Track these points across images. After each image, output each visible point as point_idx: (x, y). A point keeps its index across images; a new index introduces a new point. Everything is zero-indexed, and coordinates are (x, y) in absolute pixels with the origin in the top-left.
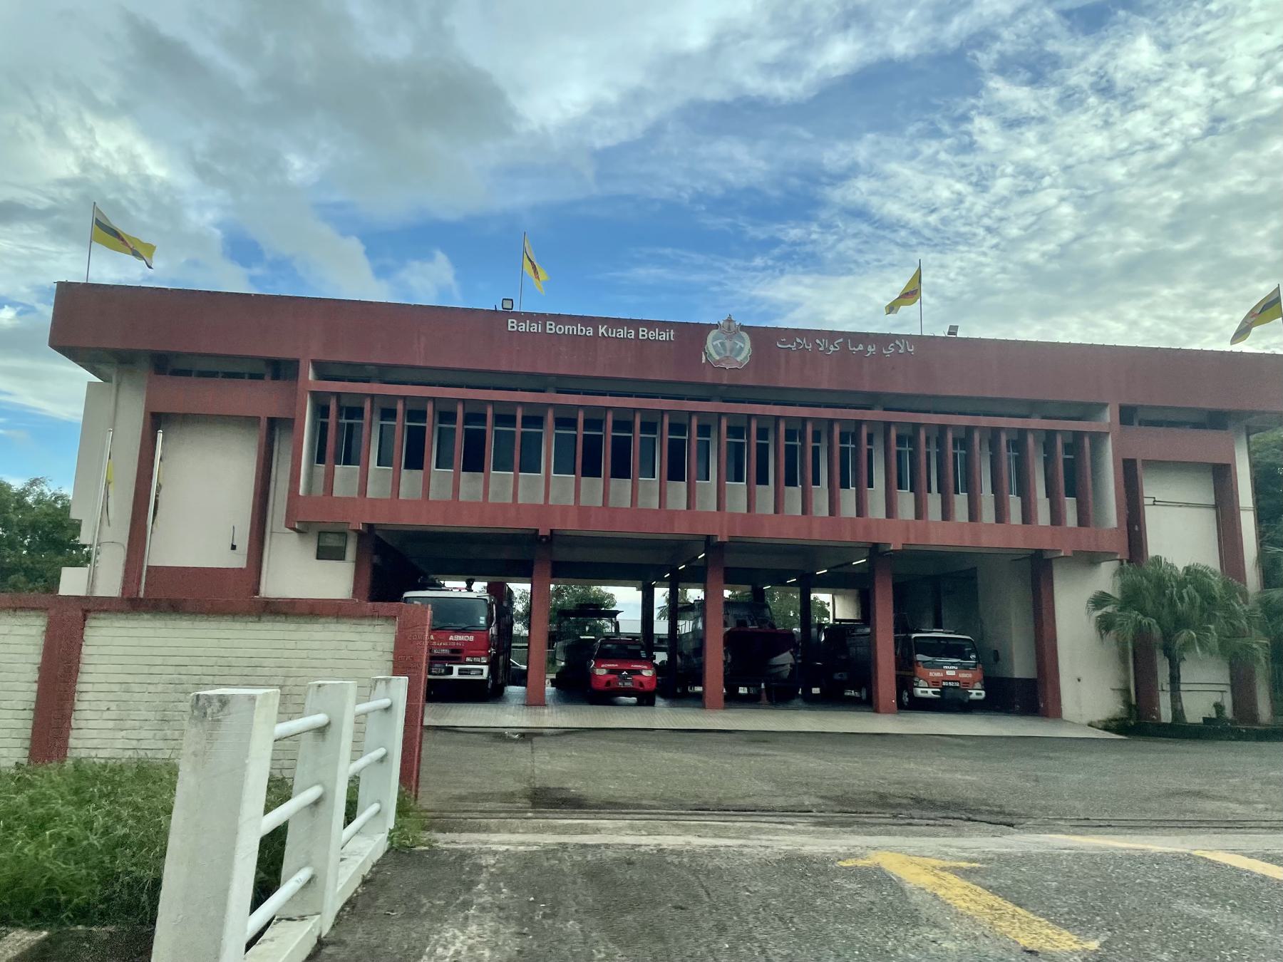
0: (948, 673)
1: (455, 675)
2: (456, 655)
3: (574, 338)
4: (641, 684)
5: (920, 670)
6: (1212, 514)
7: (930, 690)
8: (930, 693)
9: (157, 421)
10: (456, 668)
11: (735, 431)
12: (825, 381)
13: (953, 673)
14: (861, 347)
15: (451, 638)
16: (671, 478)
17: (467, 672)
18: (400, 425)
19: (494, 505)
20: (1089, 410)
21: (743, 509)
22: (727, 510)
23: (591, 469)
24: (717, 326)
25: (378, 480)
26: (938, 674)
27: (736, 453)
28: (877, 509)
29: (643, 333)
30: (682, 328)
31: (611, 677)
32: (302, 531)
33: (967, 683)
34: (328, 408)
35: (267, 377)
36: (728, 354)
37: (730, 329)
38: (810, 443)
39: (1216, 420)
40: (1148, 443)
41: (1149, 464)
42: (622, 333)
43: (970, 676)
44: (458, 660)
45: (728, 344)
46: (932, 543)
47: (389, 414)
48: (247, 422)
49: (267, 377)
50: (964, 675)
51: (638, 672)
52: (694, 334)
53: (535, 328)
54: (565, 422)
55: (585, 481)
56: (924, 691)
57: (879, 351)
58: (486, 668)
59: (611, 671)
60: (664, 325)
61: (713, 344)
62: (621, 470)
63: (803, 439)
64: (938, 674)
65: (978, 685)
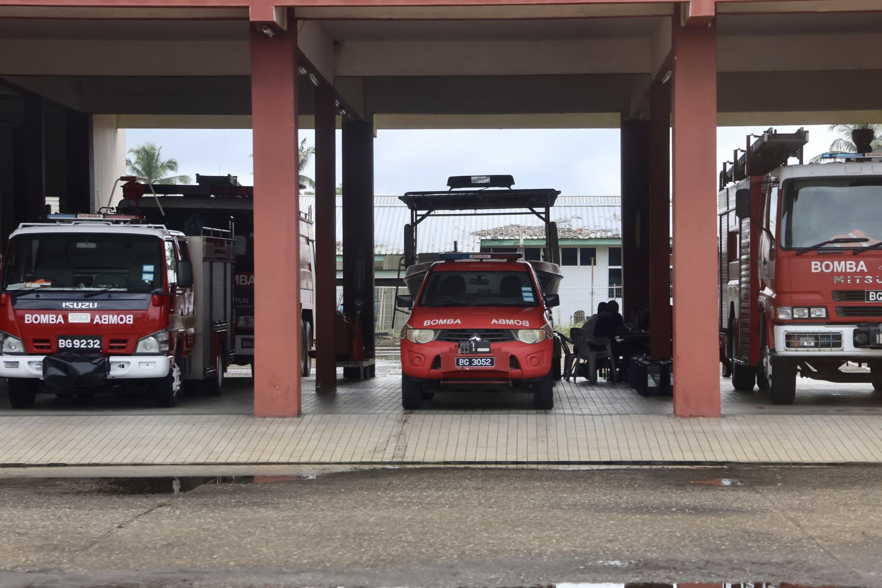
0: (73, 318)
4: (514, 361)
31: (444, 348)
51: (507, 335)
59: (446, 335)
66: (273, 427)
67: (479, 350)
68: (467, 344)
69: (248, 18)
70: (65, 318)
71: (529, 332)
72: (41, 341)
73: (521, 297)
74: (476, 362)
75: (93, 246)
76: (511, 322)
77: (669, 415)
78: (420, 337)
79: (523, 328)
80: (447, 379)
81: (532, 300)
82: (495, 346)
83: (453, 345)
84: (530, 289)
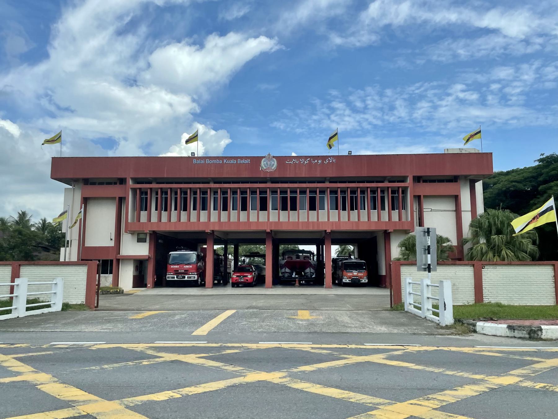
1: (186, 279)
2: (186, 272)
3: (215, 165)
4: (247, 280)
6: (454, 213)
8: (348, 281)
9: (86, 201)
10: (186, 276)
11: (393, 192)
12: (304, 174)
14: (316, 161)
15: (384, 273)
17: (190, 277)
18: (239, 196)
19: (272, 222)
20: (403, 179)
22: (393, 220)
23: (284, 208)
24: (264, 157)
25: (214, 215)
26: (351, 274)
27: (374, 199)
28: (174, 219)
29: (239, 161)
30: (253, 159)
32: (132, 233)
33: (361, 277)
34: (197, 192)
35: (118, 184)
36: (269, 167)
37: (270, 158)
38: (401, 195)
39: (454, 179)
40: (425, 189)
41: (425, 197)
42: (232, 162)
44: (187, 274)
45: (269, 163)
47: (215, 193)
48: (113, 198)
49: (118, 184)
51: (246, 276)
52: (256, 160)
53: (202, 162)
54: (234, 192)
55: (311, 212)
57: (322, 162)
58: (196, 276)
59: (237, 276)
60: (246, 158)
61: (263, 163)
62: (294, 208)
63: (398, 193)
64: (351, 274)
65: (365, 278)
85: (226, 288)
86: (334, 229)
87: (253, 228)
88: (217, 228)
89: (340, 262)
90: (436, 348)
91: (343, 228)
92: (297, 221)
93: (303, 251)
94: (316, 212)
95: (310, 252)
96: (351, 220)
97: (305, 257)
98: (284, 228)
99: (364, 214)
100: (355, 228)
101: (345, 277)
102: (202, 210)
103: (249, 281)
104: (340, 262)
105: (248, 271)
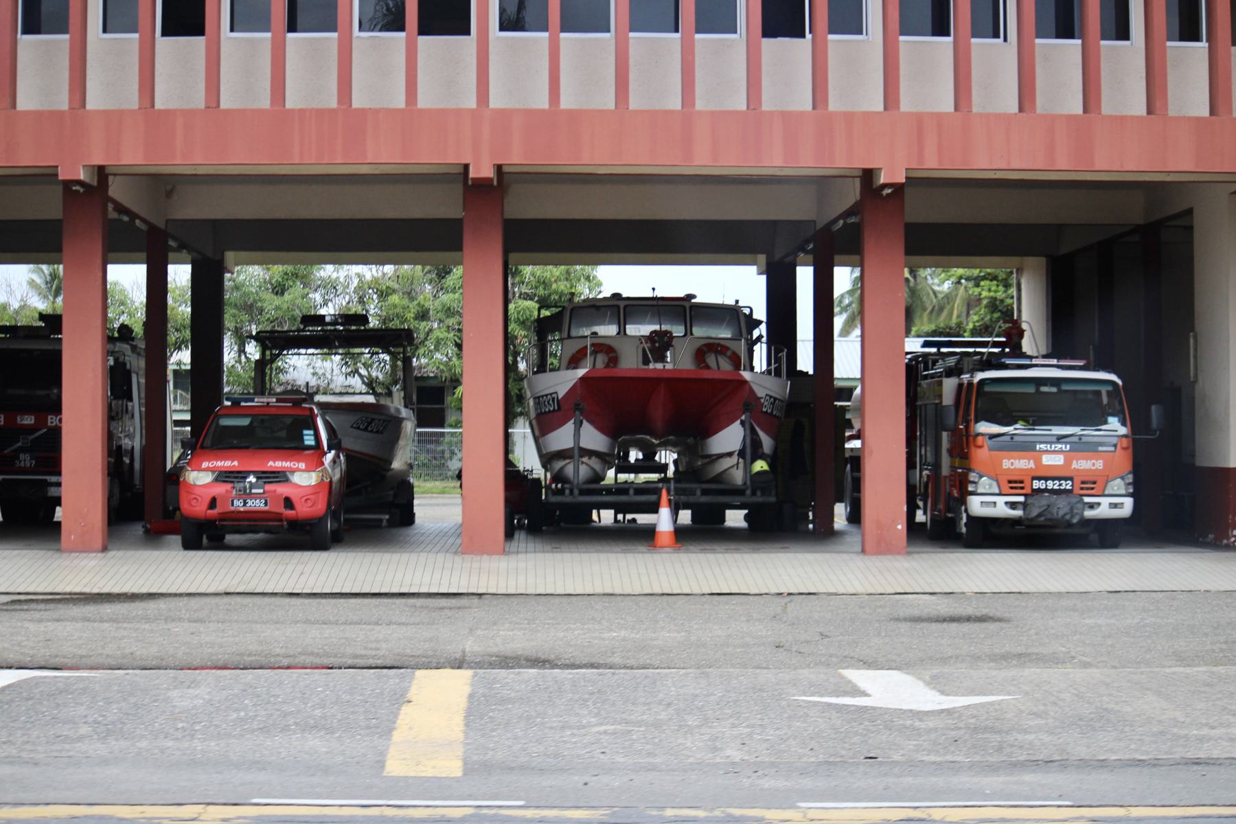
0: (1047, 460)
4: (288, 503)
5: (981, 455)
7: (1001, 500)
8: (1000, 507)
13: (1058, 460)
16: (770, 30)
19: (504, 114)
21: (945, 102)
28: (1125, 93)
31: (221, 489)
33: (1092, 484)
43: (1099, 464)
46: (125, 161)
50: (1083, 464)
51: (279, 477)
55: (774, 47)
56: (988, 502)
59: (225, 476)
65: (1118, 486)
66: (76, 562)
67: (254, 491)
68: (241, 485)
69: (57, 175)
70: (1038, 461)
71: (305, 475)
72: (1015, 482)
73: (302, 440)
74: (250, 503)
75: (1054, 390)
76: (287, 464)
77: (857, 553)
78: (197, 478)
79: (298, 470)
80: (224, 520)
81: (313, 443)
82: (268, 487)
83: (228, 486)
84: (311, 432)
85: (155, 553)
86: (932, 162)
87: (381, 154)
88: (132, 154)
89: (950, 384)
90: (770, 814)
91: (989, 158)
92: (675, 103)
93: (622, 308)
94: (607, 38)
95: (732, 314)
96: (906, 104)
97: (714, 347)
98: (595, 155)
99: (995, 60)
100: (1063, 163)
101: (985, 484)
102: (27, 30)
103: (304, 510)
104: (950, 384)
105: (290, 443)
